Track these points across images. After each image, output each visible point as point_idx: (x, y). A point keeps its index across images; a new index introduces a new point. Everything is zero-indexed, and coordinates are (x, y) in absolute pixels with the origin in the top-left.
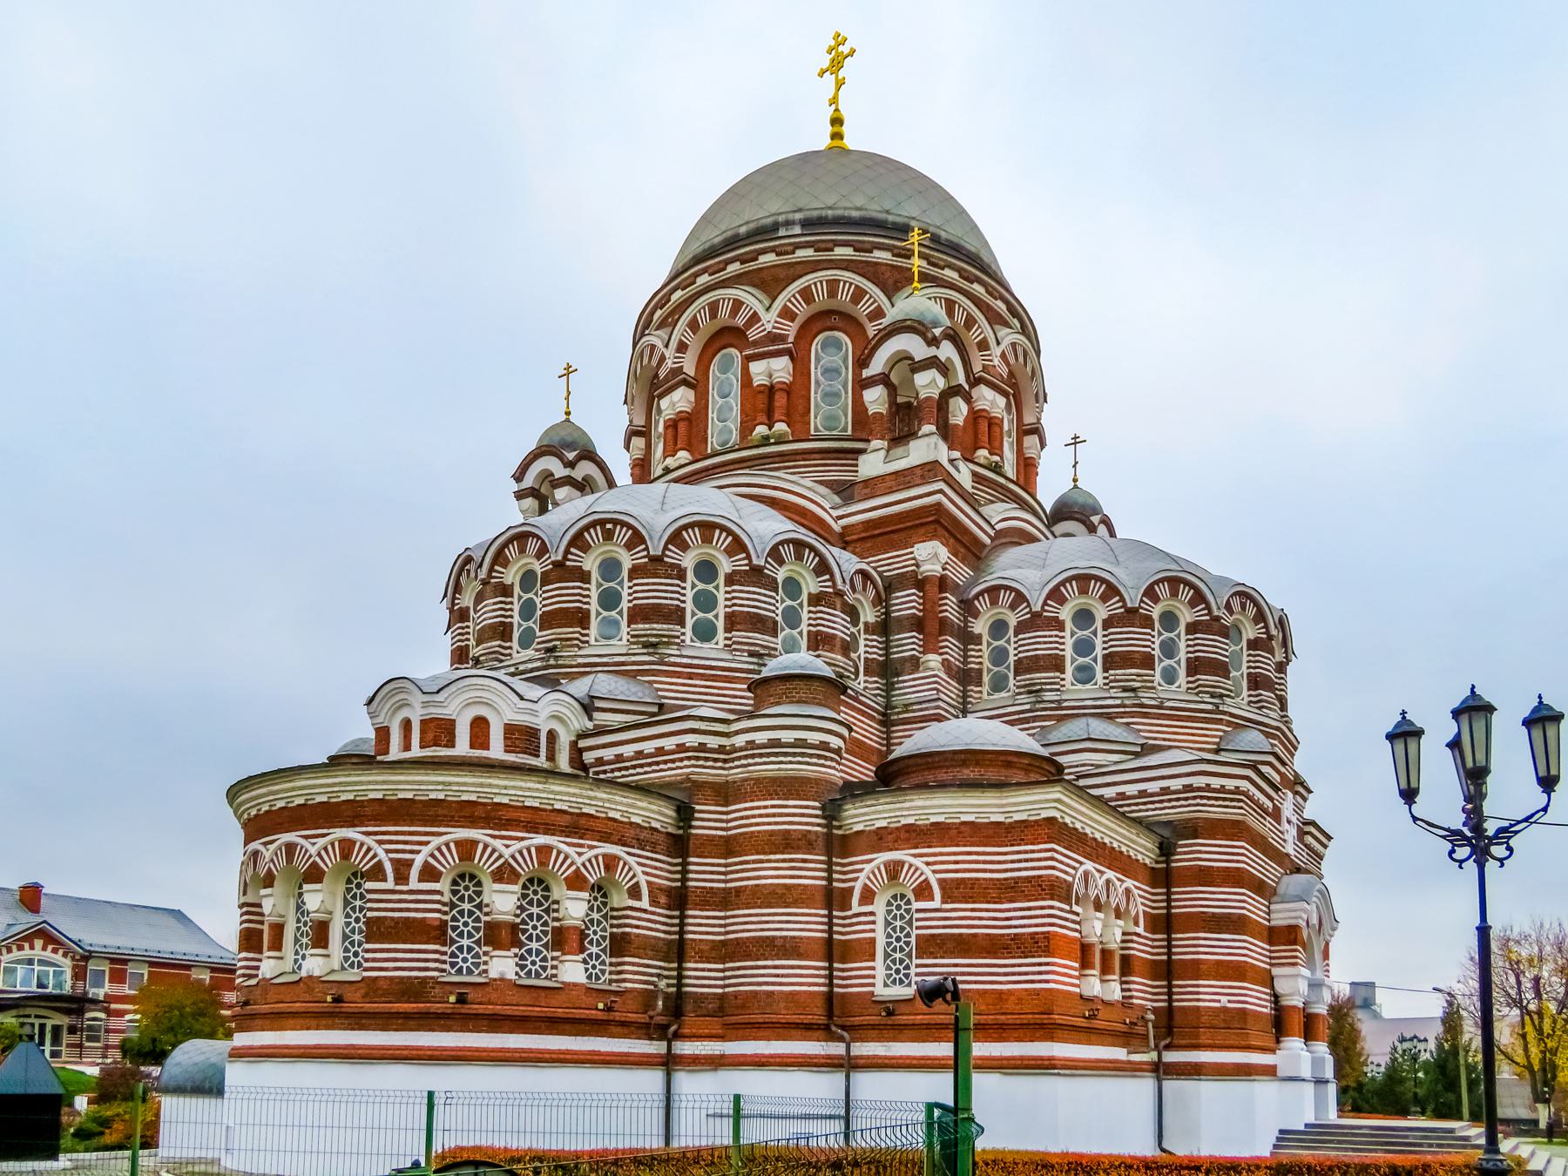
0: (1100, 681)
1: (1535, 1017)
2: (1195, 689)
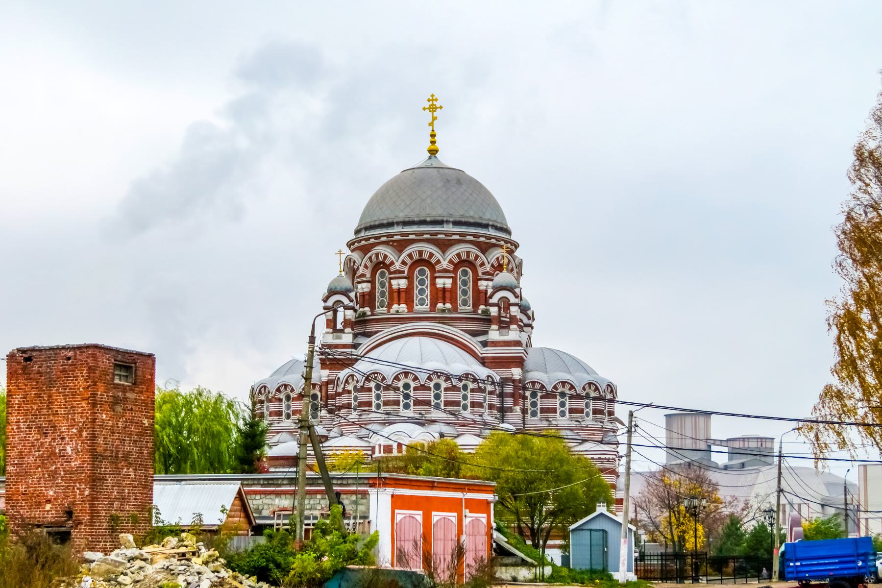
2: (571, 419)
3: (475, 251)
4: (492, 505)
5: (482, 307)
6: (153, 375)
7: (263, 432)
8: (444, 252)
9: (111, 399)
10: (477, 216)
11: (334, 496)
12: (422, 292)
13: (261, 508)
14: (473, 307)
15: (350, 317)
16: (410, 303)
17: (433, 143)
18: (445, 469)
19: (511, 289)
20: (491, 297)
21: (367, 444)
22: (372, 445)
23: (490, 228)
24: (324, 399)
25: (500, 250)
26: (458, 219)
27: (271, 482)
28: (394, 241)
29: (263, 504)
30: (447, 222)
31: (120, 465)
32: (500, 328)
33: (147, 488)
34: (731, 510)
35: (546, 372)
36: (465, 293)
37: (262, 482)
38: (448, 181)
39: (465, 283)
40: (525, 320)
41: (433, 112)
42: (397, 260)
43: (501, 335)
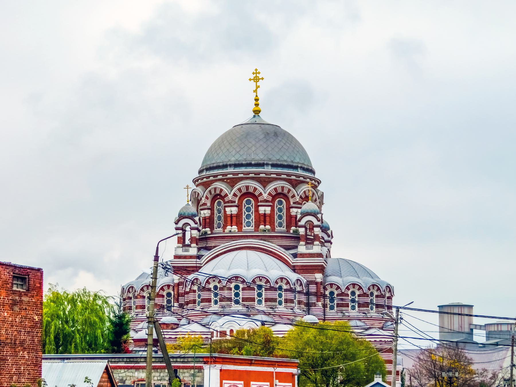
0: (357, 310)
1: (440, 381)
2: (359, 312)
3: (288, 186)
4: (296, 377)
5: (293, 228)
6: (41, 284)
7: (128, 322)
8: (265, 187)
9: (10, 302)
10: (289, 160)
11: (172, 372)
12: (248, 217)
13: (124, 379)
14: (287, 228)
15: (195, 236)
16: (239, 225)
17: (257, 105)
18: (262, 349)
19: (314, 214)
20: (299, 221)
21: (207, 330)
22: (211, 330)
23: (299, 169)
24: (176, 296)
25: (307, 186)
26: (275, 162)
27: (131, 360)
28: (227, 179)
29: (126, 376)
30: (267, 164)
31: (17, 350)
32: (307, 243)
33: (38, 366)
34: (483, 379)
35: (341, 277)
36: (280, 217)
37: (125, 360)
38: (268, 134)
39: (280, 210)
40: (326, 238)
41: (257, 82)
42: (230, 193)
43: (307, 248)
